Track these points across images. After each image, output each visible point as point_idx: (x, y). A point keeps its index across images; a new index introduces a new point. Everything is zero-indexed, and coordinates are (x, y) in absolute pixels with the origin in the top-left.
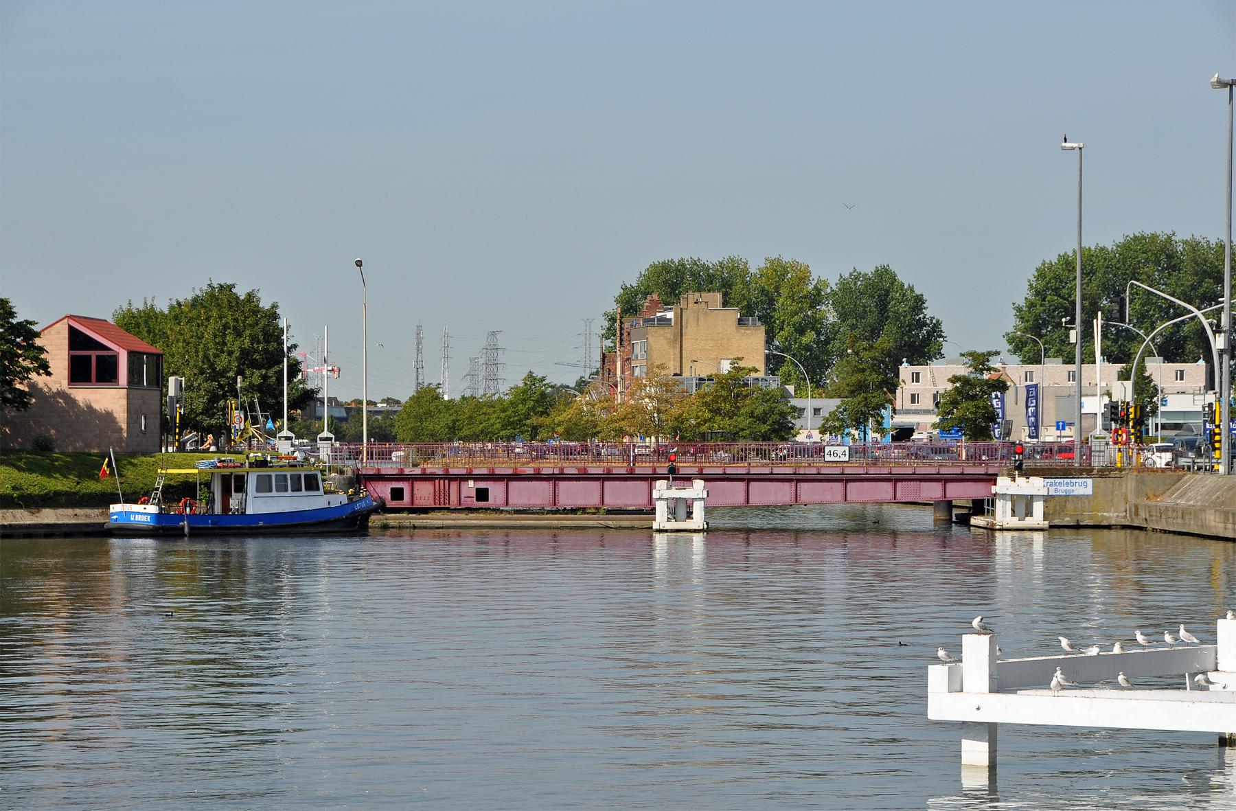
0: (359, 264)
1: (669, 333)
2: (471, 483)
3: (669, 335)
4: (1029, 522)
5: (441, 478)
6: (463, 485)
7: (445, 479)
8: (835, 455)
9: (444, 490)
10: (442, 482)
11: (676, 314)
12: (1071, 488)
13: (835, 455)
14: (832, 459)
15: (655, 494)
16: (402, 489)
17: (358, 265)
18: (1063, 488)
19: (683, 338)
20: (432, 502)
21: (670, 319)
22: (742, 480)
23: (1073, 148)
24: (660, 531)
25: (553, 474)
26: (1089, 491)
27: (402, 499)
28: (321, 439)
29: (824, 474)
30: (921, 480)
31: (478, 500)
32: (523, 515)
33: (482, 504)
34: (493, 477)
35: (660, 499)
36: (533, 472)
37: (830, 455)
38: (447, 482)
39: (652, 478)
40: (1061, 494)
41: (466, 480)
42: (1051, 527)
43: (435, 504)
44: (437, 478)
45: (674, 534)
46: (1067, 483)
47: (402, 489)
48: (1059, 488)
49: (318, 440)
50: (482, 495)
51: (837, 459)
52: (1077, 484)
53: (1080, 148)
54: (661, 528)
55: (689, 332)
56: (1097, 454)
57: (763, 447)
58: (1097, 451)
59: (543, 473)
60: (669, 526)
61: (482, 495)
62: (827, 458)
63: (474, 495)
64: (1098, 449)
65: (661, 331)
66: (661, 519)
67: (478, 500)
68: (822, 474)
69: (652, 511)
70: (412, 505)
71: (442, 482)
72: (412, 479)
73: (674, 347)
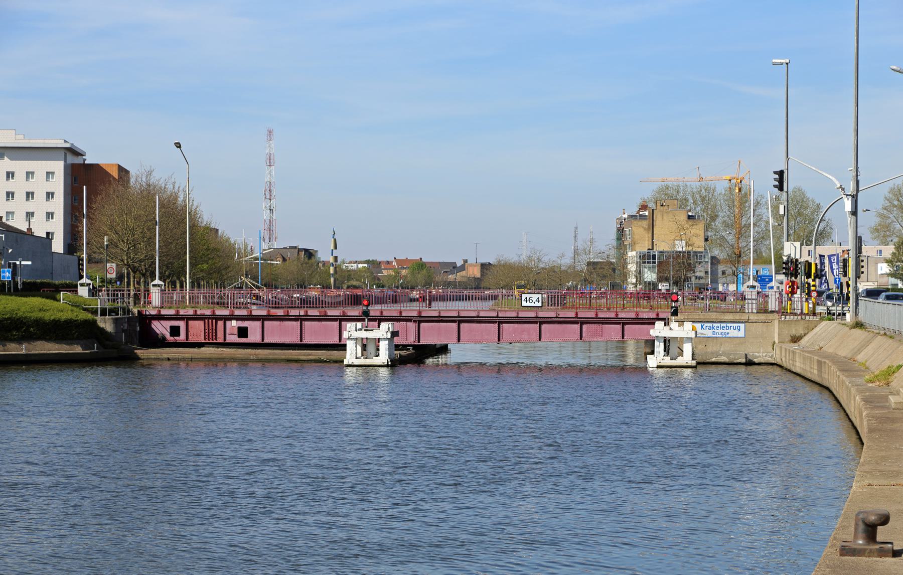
0: (178, 145)
1: (645, 223)
2: (234, 323)
3: (645, 226)
4: (680, 361)
5: (209, 318)
6: (228, 323)
7: (212, 319)
8: (531, 301)
9: (212, 328)
10: (210, 321)
11: (649, 213)
12: (727, 331)
13: (531, 301)
14: (528, 304)
15: (345, 335)
16: (179, 327)
17: (177, 147)
18: (720, 331)
19: (655, 229)
20: (203, 337)
21: (647, 216)
22: (494, 322)
23: (782, 64)
24: (349, 366)
25: (300, 316)
26: (741, 334)
27: (179, 335)
28: (154, 286)
29: (522, 317)
30: (603, 323)
31: (239, 337)
32: (305, 351)
33: (243, 340)
34: (251, 318)
35: (349, 338)
36: (283, 314)
37: (527, 301)
38: (214, 321)
39: (342, 319)
40: (718, 336)
41: (231, 319)
42: (698, 363)
43: (205, 339)
44: (206, 318)
45: (668, 369)
46: (723, 328)
47: (179, 327)
48: (716, 331)
49: (78, 285)
50: (243, 332)
51: (532, 305)
52: (732, 328)
53: (787, 64)
54: (350, 363)
55: (658, 223)
56: (750, 301)
57: (458, 294)
58: (750, 299)
59: (290, 314)
60: (356, 362)
61: (243, 332)
62: (524, 304)
63: (236, 332)
64: (750, 297)
65: (640, 223)
66: (352, 354)
67: (239, 337)
68: (520, 317)
69: (343, 347)
70: (419, 342)
71: (210, 321)
72: (187, 319)
73: (648, 233)
